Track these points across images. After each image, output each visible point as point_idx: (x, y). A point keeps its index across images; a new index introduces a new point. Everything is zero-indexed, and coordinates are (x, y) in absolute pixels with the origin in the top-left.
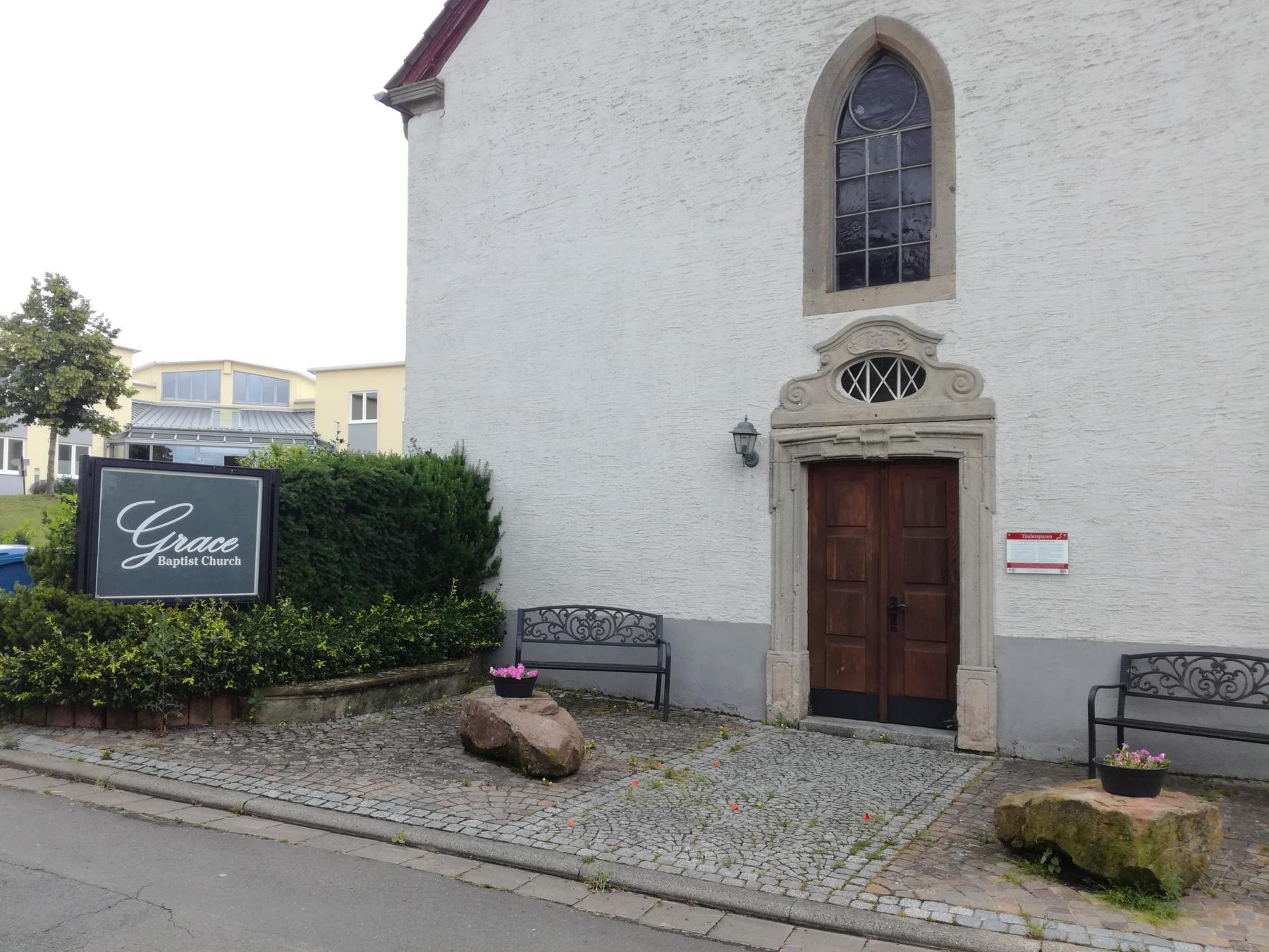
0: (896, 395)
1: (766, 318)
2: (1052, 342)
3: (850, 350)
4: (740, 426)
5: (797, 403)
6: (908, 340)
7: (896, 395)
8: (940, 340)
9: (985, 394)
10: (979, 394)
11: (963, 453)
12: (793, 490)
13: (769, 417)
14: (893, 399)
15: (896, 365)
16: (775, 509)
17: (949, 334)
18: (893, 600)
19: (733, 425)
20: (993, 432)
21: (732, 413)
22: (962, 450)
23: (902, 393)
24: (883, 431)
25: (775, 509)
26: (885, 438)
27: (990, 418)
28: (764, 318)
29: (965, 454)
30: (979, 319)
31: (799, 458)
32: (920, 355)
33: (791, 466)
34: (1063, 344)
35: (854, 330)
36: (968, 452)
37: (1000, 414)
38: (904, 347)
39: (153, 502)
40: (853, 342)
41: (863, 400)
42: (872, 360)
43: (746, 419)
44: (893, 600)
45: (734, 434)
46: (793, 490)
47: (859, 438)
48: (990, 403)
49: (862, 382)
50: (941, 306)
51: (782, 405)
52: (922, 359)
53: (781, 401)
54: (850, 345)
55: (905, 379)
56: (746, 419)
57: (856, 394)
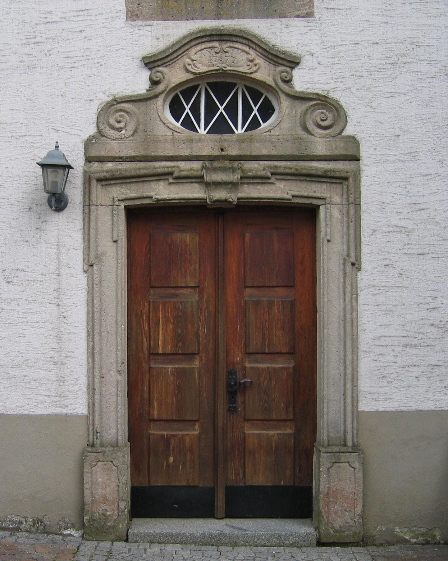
0: (237, 129)
1: (76, 19)
2: (420, 77)
3: (189, 68)
4: (49, 155)
5: (119, 130)
6: (260, 61)
7: (237, 129)
8: (298, 64)
9: (349, 131)
10: (342, 131)
11: (324, 199)
12: (116, 242)
13: (81, 147)
14: (234, 132)
15: (236, 94)
16: (92, 265)
17: (308, 57)
18: (231, 373)
19: (41, 155)
20: (357, 174)
21: (29, 139)
22: (324, 195)
23: (242, 128)
24: (233, 170)
25: (92, 265)
26: (235, 177)
27: (356, 158)
28: (72, 19)
29: (328, 200)
30: (340, 43)
31: (122, 200)
32: (274, 80)
33: (113, 210)
34: (431, 80)
35: (194, 43)
36: (330, 197)
37: (365, 152)
38: (254, 69)
39: (282, 481)
40: (194, 58)
41: (197, 132)
42: (208, 84)
43: (57, 147)
44: (231, 373)
45: (43, 166)
46: (116, 242)
47: (202, 177)
48: (354, 141)
49: (195, 109)
50: (298, 24)
51: (100, 133)
52: (277, 84)
53: (98, 127)
54: (188, 61)
55: (247, 110)
56: (57, 147)
57: (188, 124)
